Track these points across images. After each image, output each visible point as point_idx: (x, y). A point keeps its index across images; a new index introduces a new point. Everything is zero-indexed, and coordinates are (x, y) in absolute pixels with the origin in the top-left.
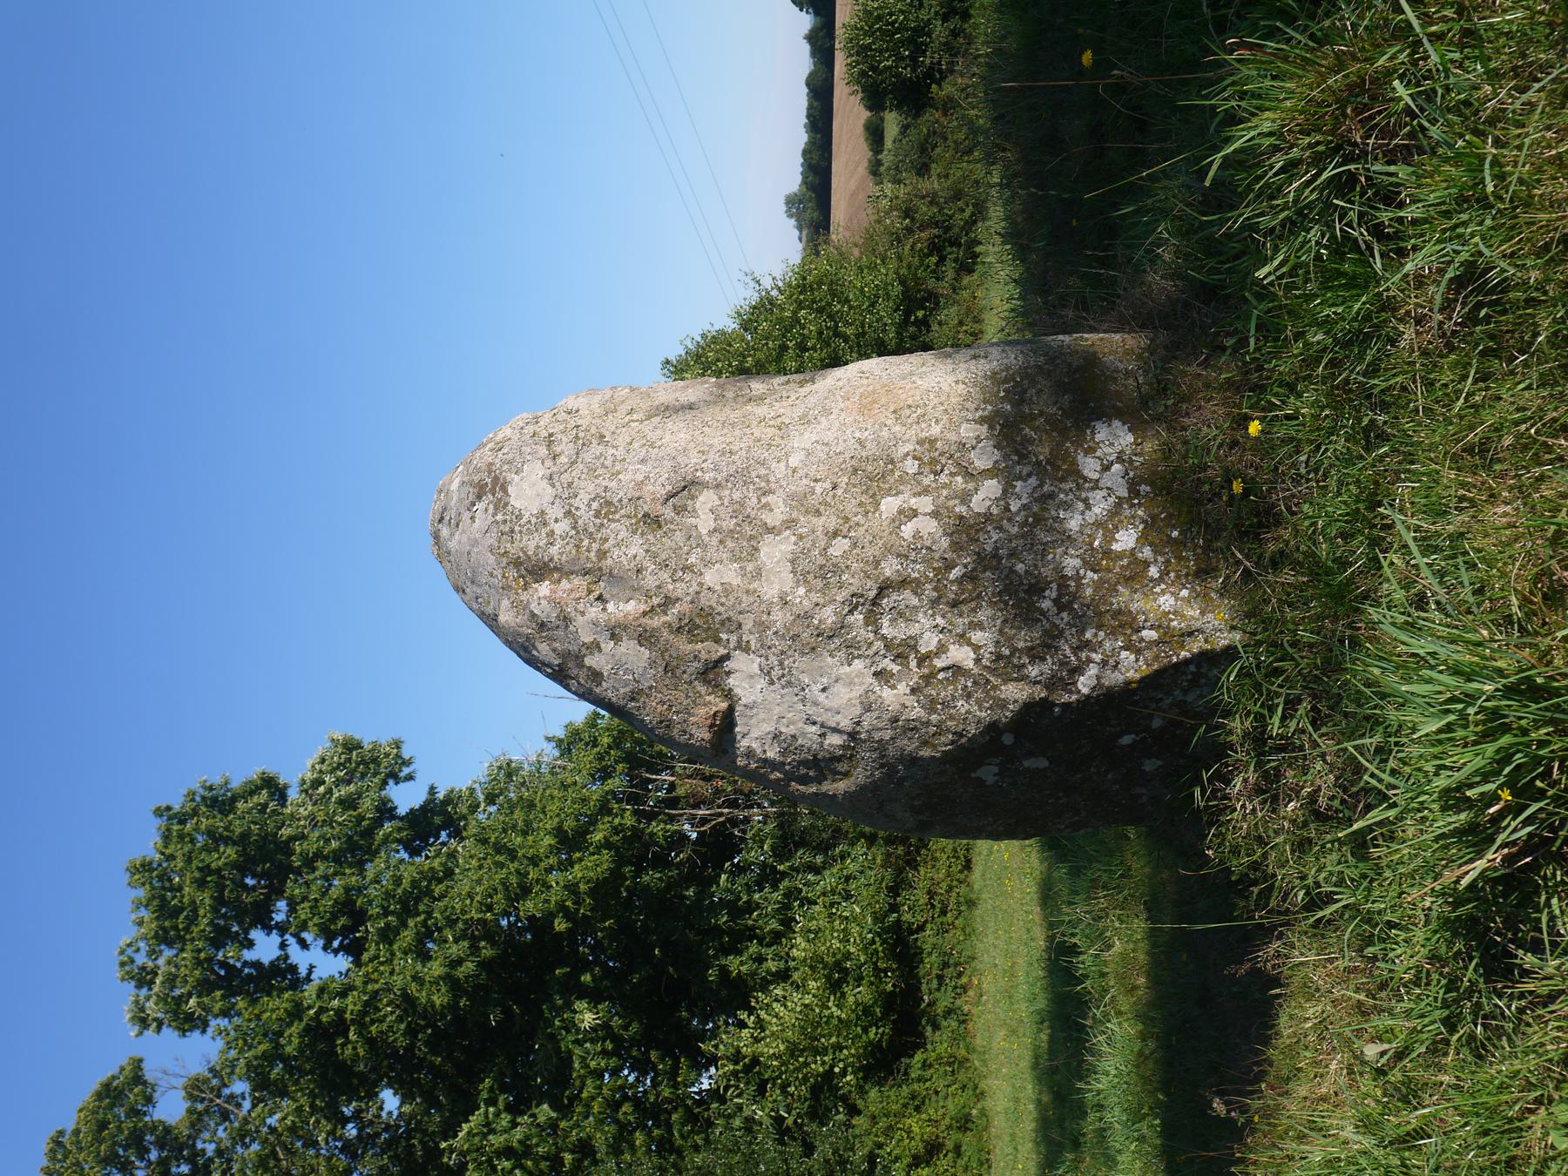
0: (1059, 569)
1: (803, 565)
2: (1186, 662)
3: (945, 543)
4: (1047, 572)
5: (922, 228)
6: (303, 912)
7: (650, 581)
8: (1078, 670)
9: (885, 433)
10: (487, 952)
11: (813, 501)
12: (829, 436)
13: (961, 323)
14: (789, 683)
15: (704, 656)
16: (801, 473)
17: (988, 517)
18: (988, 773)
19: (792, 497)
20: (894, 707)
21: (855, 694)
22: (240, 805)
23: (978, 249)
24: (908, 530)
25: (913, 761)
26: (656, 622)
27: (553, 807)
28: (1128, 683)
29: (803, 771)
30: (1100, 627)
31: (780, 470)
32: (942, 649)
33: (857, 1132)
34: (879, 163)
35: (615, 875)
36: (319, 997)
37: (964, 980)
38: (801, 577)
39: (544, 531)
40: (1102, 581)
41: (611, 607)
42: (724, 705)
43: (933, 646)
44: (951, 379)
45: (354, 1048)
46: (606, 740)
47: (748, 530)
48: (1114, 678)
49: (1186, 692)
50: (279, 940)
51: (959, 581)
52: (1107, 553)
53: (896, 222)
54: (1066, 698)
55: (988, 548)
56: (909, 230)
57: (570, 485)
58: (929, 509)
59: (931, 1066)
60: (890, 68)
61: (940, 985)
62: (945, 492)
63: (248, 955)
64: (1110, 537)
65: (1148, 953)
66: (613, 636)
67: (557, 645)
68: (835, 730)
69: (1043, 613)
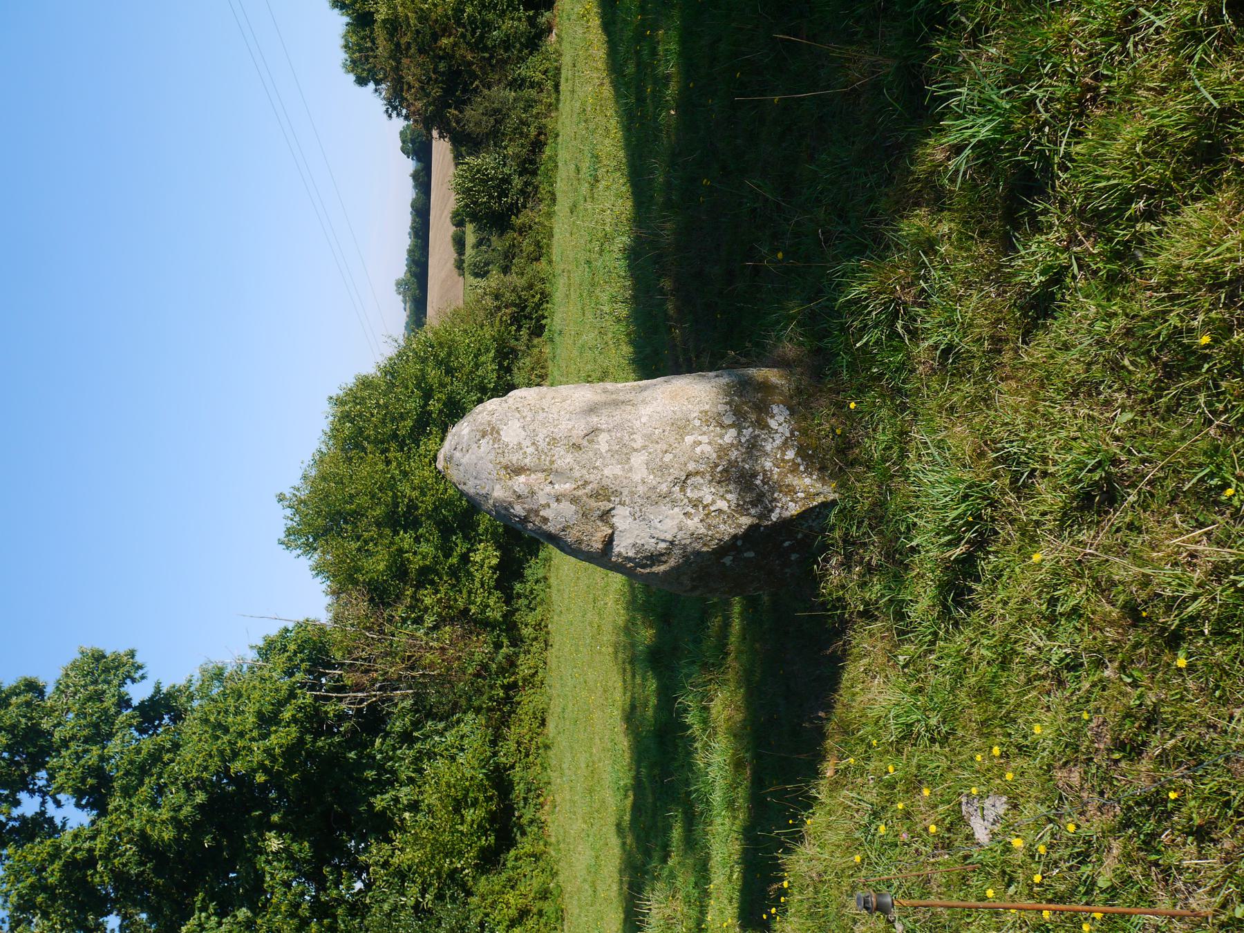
0: (763, 467)
1: (652, 465)
2: (816, 506)
3: (715, 455)
4: (758, 468)
5: (506, 307)
6: (60, 778)
7: (577, 474)
8: (772, 511)
9: (684, 408)
10: (200, 797)
11: (655, 437)
12: (659, 409)
13: (533, 369)
14: (644, 519)
15: (602, 508)
17: (732, 445)
18: (728, 560)
19: (645, 435)
20: (692, 529)
21: (675, 523)
22: (14, 700)
23: (543, 322)
25: (698, 553)
26: (580, 492)
27: (256, 695)
28: (792, 516)
29: (645, 562)
30: (780, 492)
32: (714, 502)
33: (472, 907)
34: (462, 261)
35: (301, 741)
36: (73, 841)
37: (542, 799)
38: (651, 471)
39: (521, 452)
40: (781, 472)
41: (556, 486)
42: (610, 531)
43: (709, 501)
45: (101, 877)
46: (292, 647)
47: (625, 450)
48: (787, 514)
49: (813, 521)
50: (41, 800)
51: (721, 472)
52: (783, 460)
53: (489, 302)
54: (766, 523)
55: (733, 458)
56: (499, 308)
57: (534, 430)
58: (707, 441)
59: (521, 858)
60: (485, 203)
61: (525, 804)
63: (16, 812)
64: (784, 454)
66: (557, 500)
67: (526, 506)
68: (663, 541)
69: (756, 486)
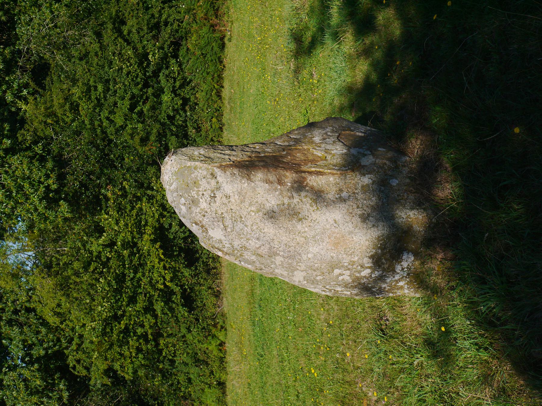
16: (311, 260)
24: (341, 278)
31: (304, 257)
44: (364, 239)
62: (354, 270)
65: (412, 209)
